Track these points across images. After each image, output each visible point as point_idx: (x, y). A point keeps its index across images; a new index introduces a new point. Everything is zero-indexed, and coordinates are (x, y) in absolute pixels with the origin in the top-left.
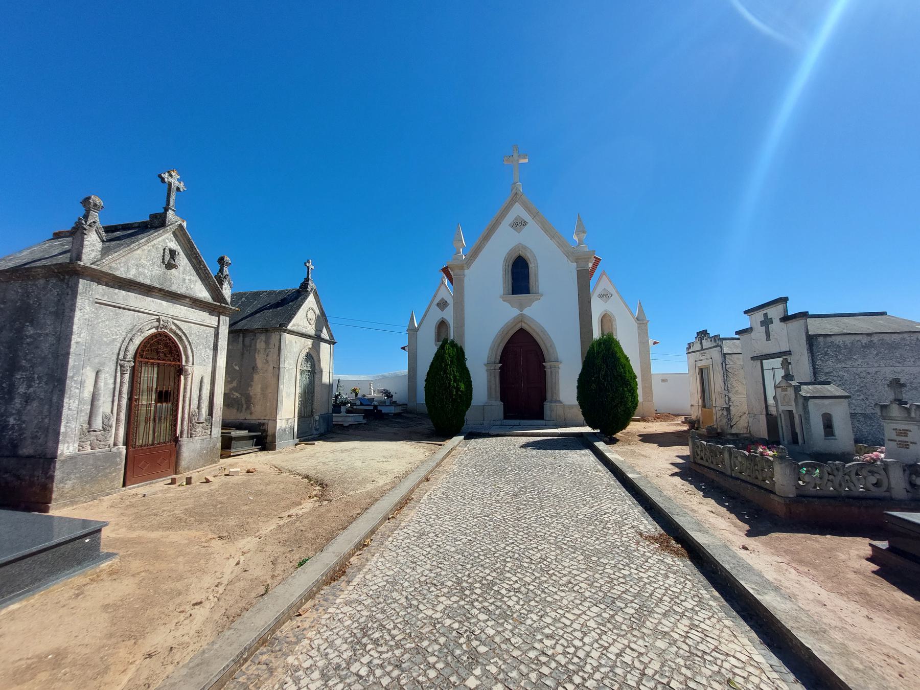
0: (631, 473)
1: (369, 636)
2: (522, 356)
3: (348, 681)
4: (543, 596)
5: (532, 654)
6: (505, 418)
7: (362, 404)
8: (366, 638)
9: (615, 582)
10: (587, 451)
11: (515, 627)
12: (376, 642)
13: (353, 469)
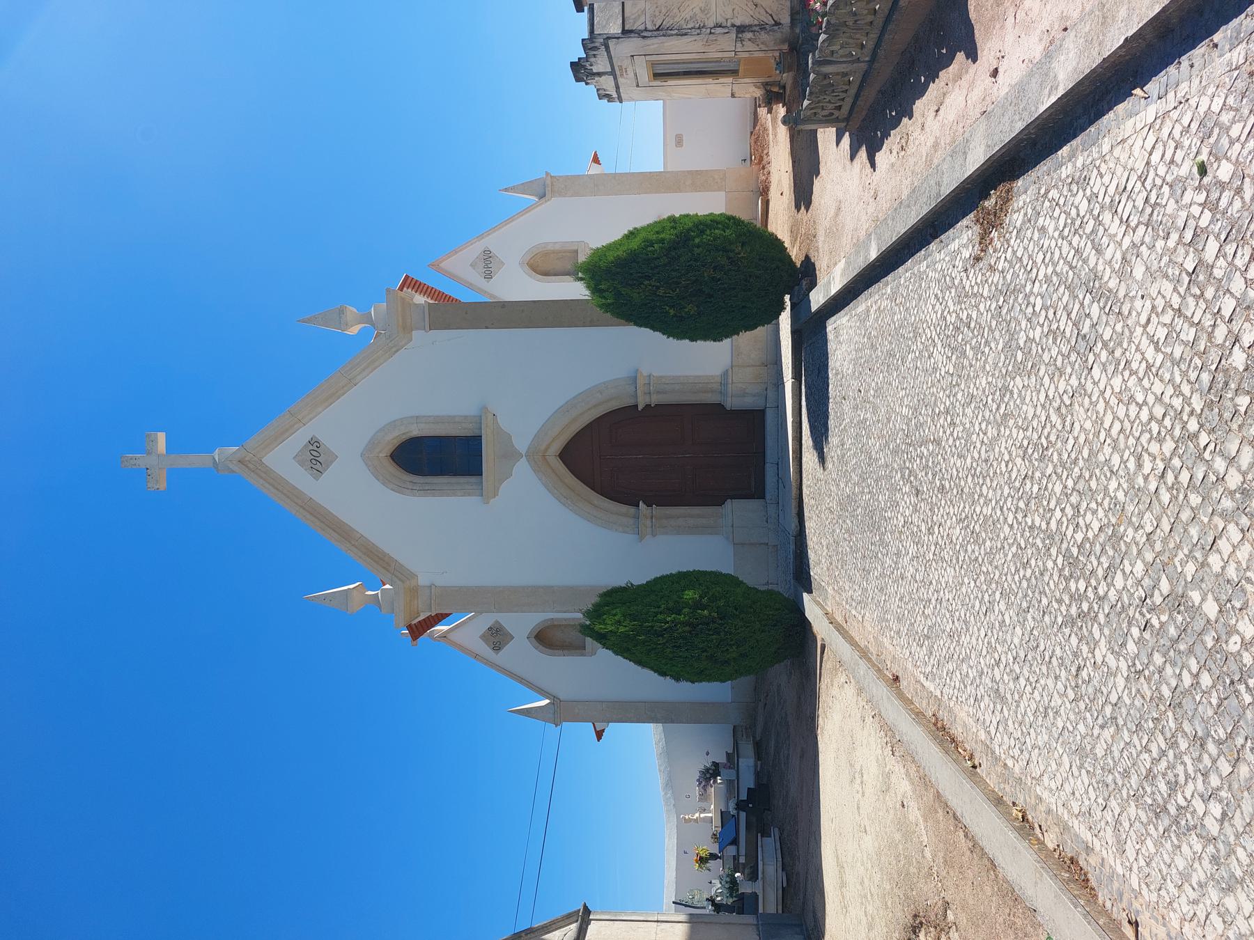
0: (868, 251)
1: (1166, 803)
2: (621, 456)
3: (1232, 839)
4: (1081, 463)
5: (1165, 497)
6: (762, 496)
7: (735, 842)
8: (1169, 806)
9: (1054, 327)
10: (831, 325)
11: (1130, 522)
12: (1173, 787)
13: (879, 854)
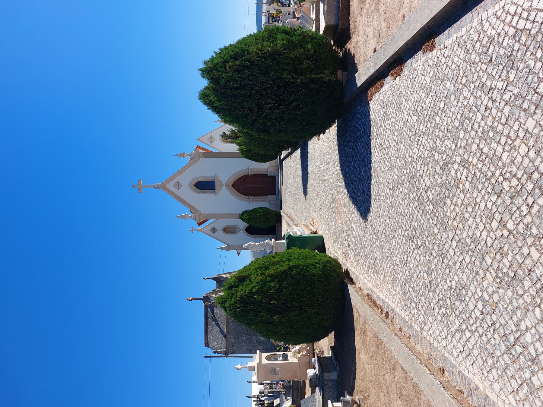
2: (245, 185)
10: (284, 162)
